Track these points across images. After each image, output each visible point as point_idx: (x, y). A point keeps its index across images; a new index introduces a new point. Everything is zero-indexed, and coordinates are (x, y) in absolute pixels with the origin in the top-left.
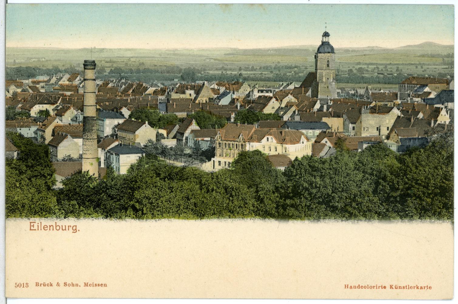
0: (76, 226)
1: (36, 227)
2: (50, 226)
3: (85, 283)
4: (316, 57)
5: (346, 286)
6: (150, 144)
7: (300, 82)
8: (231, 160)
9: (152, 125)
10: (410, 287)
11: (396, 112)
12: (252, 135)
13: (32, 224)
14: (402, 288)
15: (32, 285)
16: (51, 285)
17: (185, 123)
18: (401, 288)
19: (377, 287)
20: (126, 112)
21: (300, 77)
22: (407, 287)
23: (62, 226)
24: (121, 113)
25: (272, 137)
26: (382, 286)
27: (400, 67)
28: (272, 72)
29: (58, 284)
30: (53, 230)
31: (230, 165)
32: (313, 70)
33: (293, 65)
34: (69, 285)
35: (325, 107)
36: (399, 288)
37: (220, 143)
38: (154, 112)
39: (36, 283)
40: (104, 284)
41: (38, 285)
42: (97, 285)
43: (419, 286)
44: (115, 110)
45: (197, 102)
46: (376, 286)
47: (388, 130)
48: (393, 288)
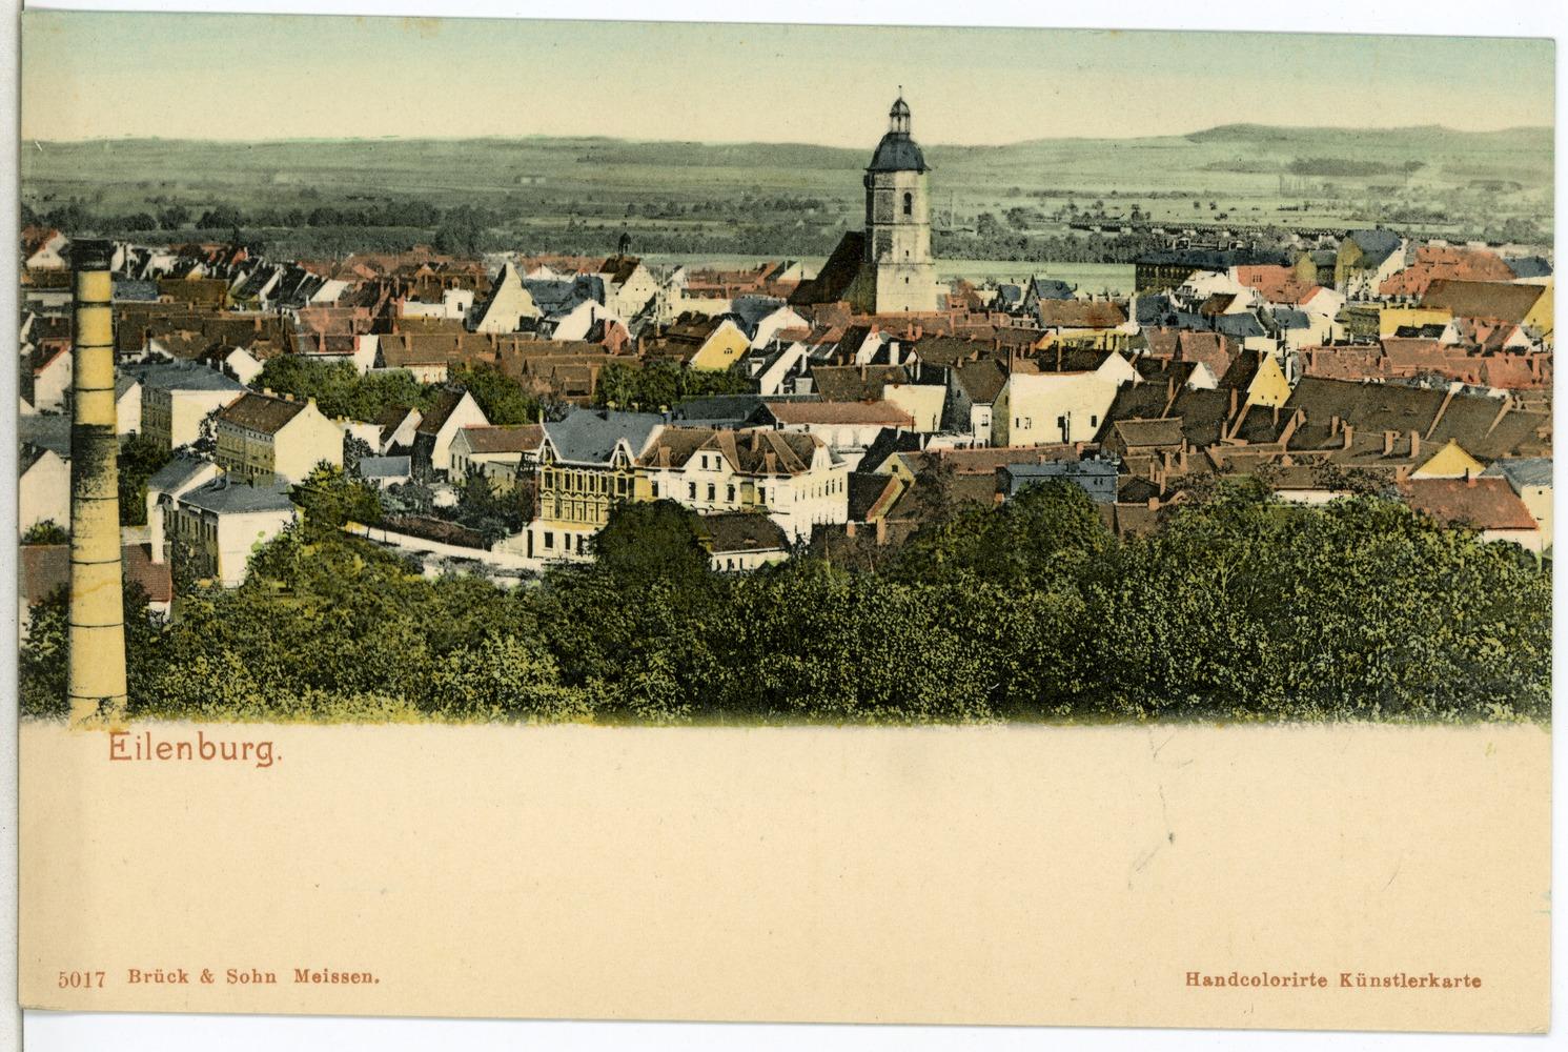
0: (270, 745)
1: (130, 750)
3: (298, 971)
4: (869, 182)
5: (1192, 978)
6: (323, 474)
7: (823, 255)
8: (588, 531)
9: (330, 410)
10: (1407, 980)
11: (1116, 370)
12: (655, 449)
13: (118, 740)
14: (1382, 982)
15: (286, 976)
16: (183, 978)
17: (440, 403)
18: (1223, 984)
19: (1297, 981)
20: (245, 364)
21: (823, 239)
22: (1400, 981)
24: (229, 371)
25: (719, 454)
26: (1312, 977)
27: (1145, 206)
28: (733, 222)
29: (206, 977)
31: (585, 544)
32: (856, 221)
33: (804, 199)
34: (245, 978)
35: (895, 348)
36: (1373, 985)
37: (549, 476)
38: (341, 364)
39: (132, 971)
40: (365, 975)
41: (139, 980)
42: (340, 978)
43: (1441, 976)
44: (209, 361)
45: (482, 328)
46: (1292, 976)
47: (1094, 423)
48: (1349, 985)
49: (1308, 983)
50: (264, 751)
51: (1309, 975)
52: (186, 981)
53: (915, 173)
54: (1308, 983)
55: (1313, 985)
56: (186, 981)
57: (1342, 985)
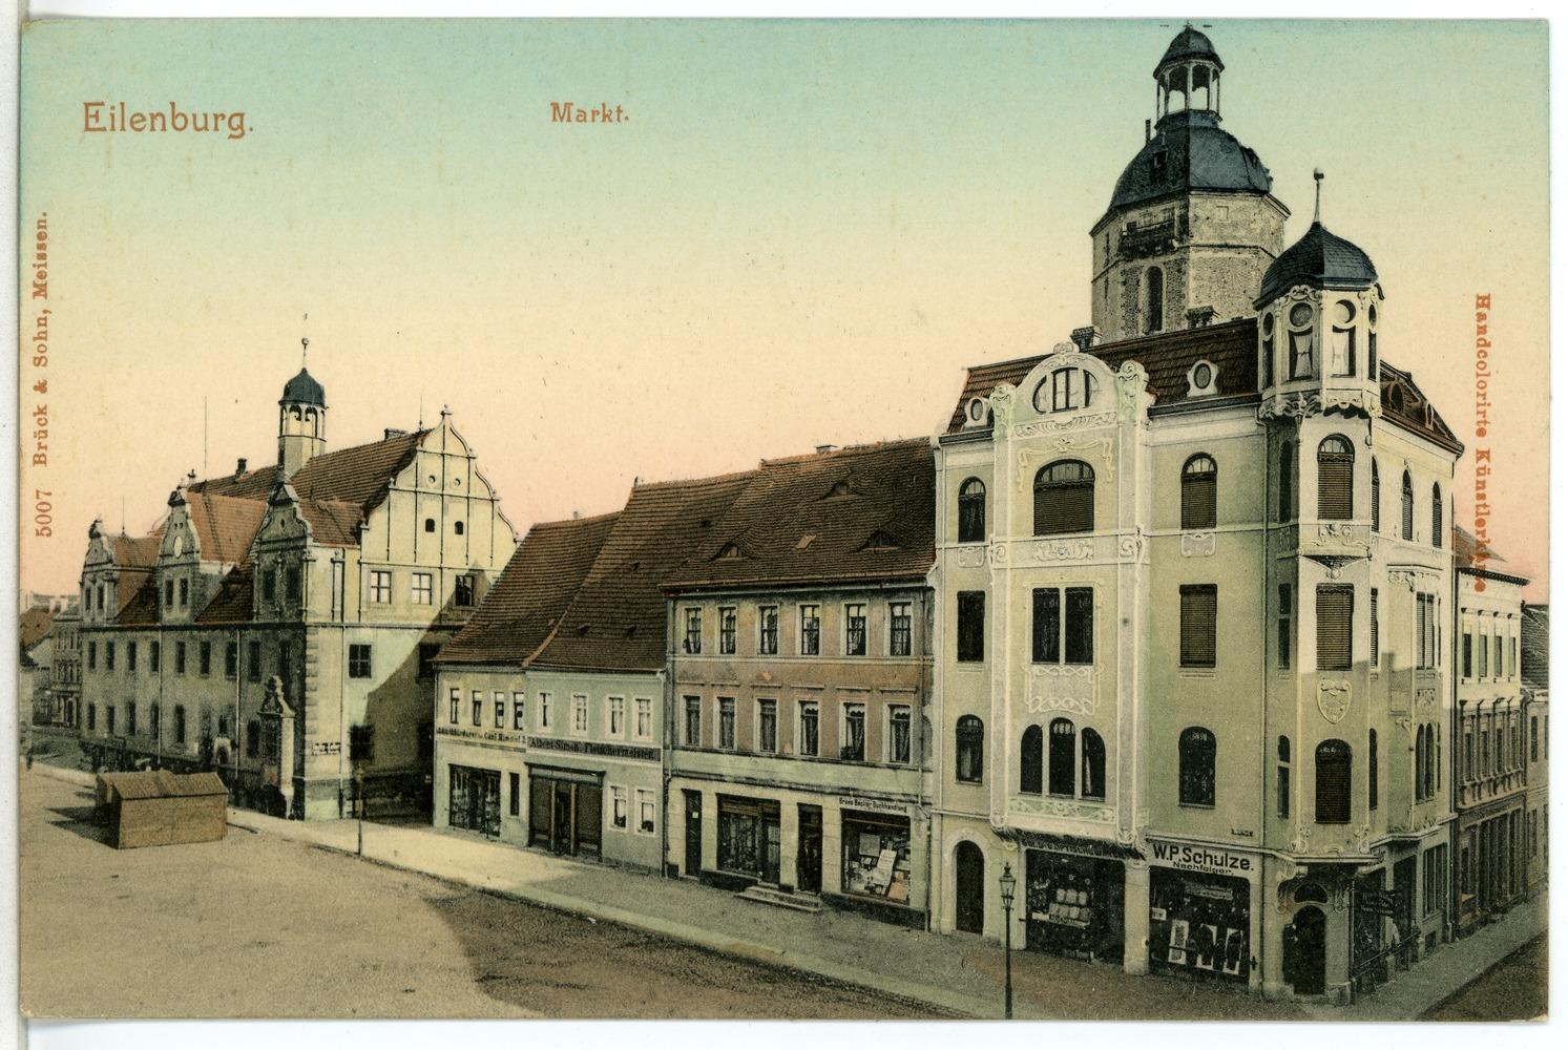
0: (241, 115)
1: (105, 121)
2: (153, 117)
10: (1483, 517)
22: (1482, 510)
23: (195, 116)
30: (164, 129)
34: (42, 349)
41: (43, 455)
48: (1478, 459)
49: (1480, 418)
50: (236, 121)
51: (1487, 419)
52: (45, 408)
53: (605, 778)
54: (1480, 418)
55: (1478, 422)
56: (45, 408)
57: (1478, 452)
